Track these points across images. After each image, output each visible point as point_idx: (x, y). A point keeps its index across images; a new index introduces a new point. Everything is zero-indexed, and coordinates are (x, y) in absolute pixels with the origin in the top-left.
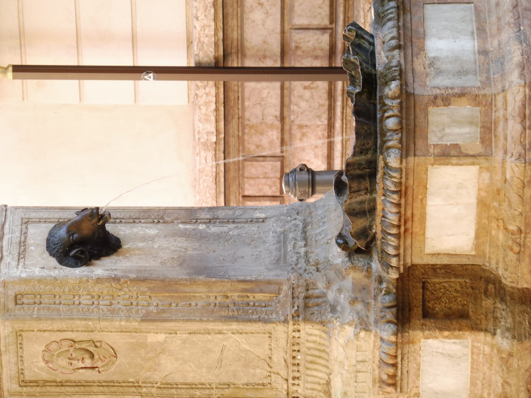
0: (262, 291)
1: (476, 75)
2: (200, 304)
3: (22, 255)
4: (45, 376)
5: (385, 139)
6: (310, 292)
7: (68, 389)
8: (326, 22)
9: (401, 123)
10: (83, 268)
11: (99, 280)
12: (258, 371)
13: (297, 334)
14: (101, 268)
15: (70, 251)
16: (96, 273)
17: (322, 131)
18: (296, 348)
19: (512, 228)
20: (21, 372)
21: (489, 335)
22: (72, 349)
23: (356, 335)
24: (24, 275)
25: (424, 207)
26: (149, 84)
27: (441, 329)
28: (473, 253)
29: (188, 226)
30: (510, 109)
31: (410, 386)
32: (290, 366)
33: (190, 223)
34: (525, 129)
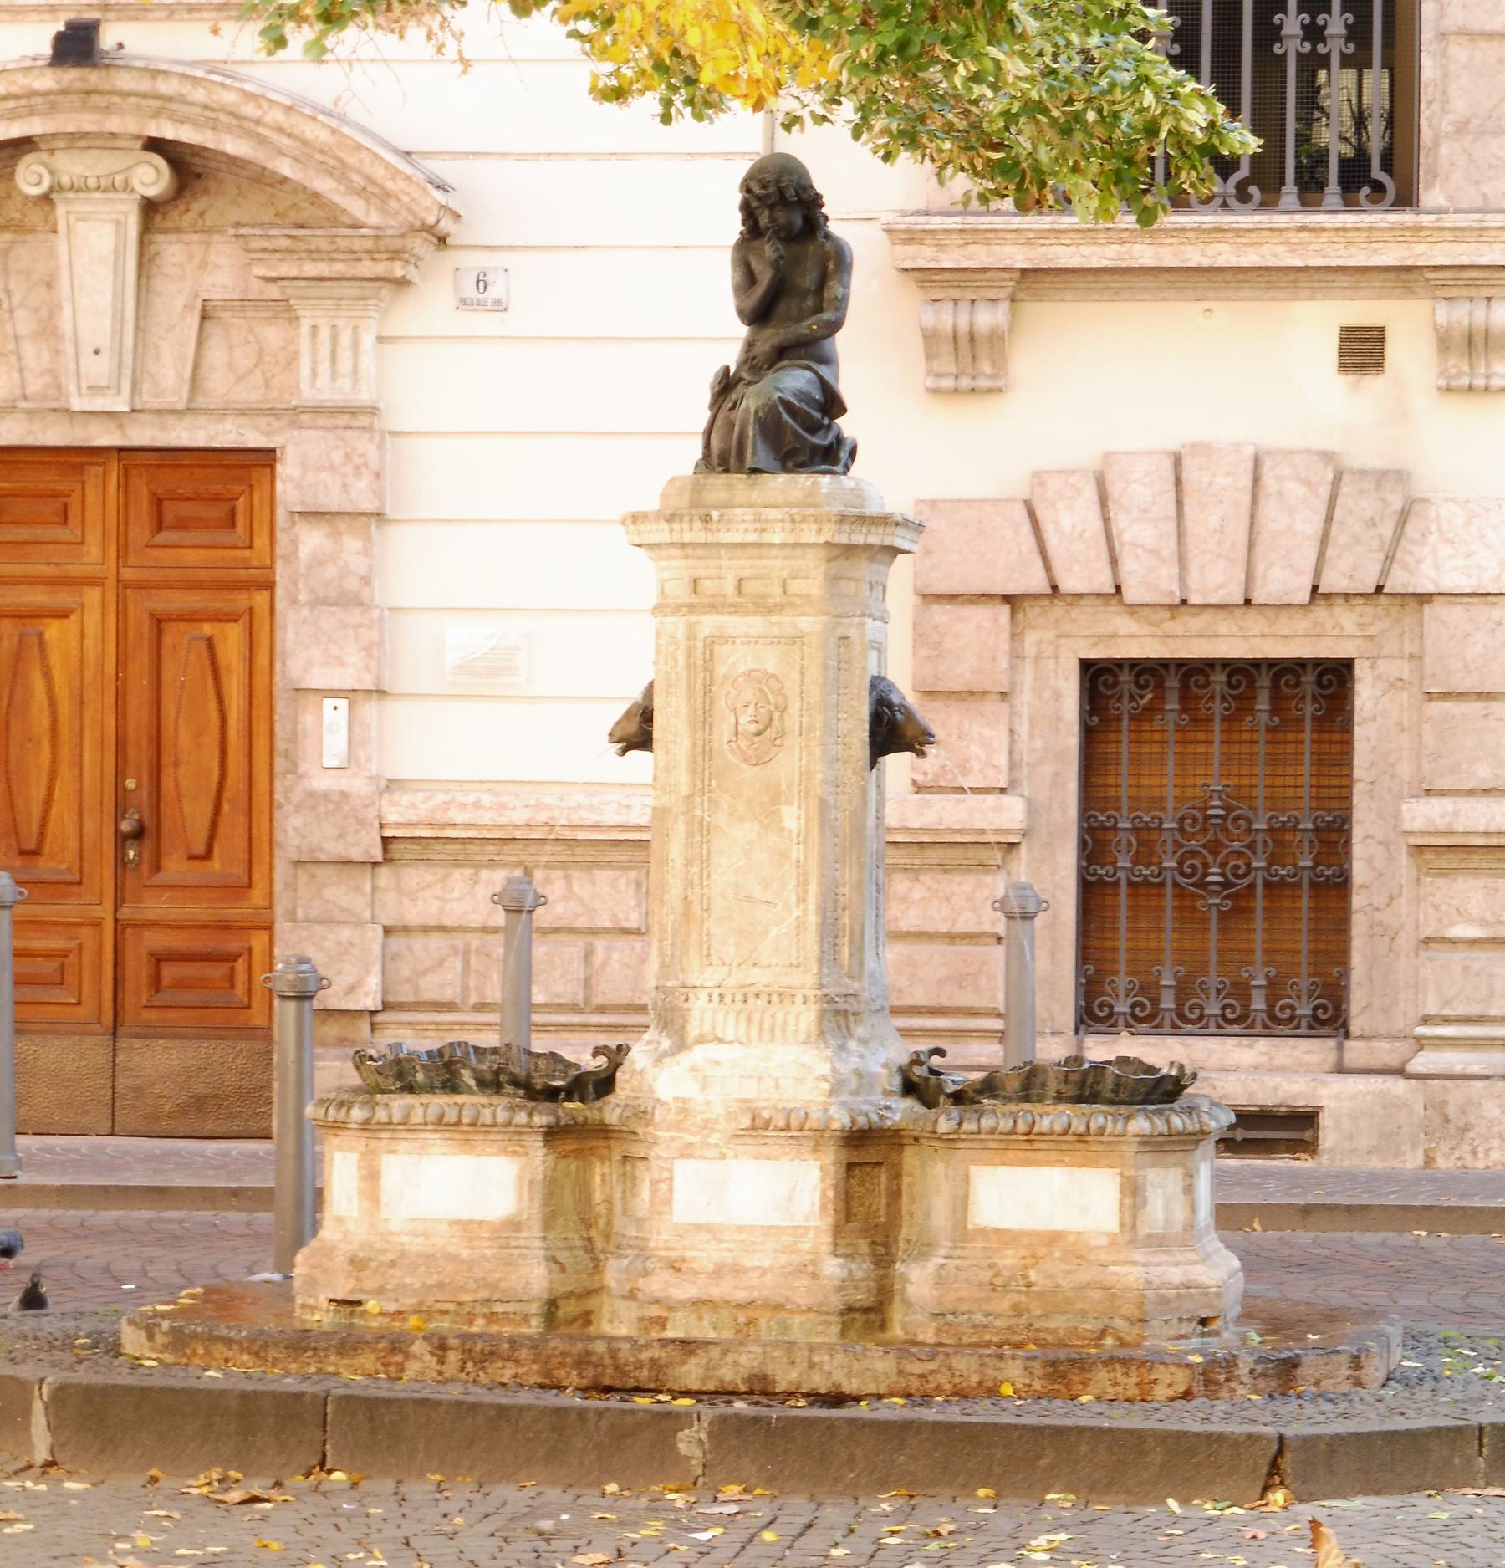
0: (851, 955)
2: (837, 874)
6: (852, 1018)
7: (700, 700)
8: (598, 1000)
9: (1179, 1134)
12: (732, 949)
13: (799, 1000)
18: (775, 998)
19: (1033, 1275)
20: (729, 640)
21: (830, 1248)
23: (824, 1078)
28: (970, 1227)
31: (740, 1148)
32: (744, 990)
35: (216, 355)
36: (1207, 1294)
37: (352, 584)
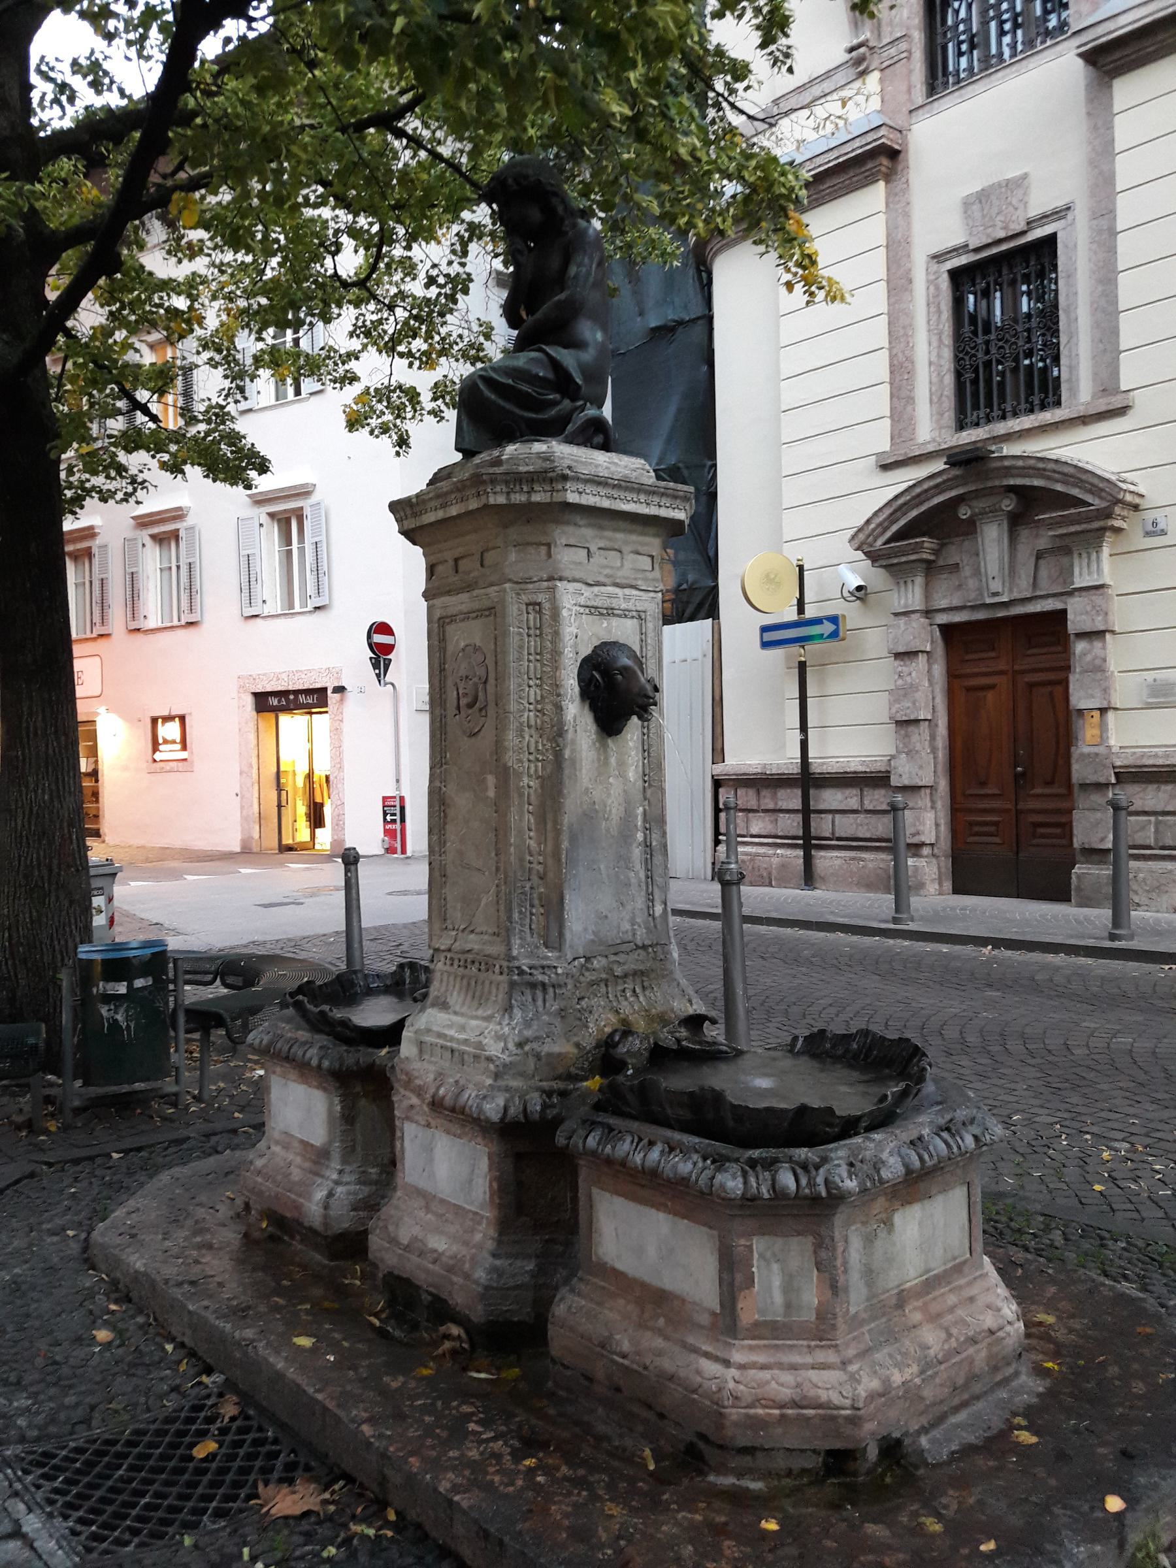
1: (868, 1300)
3: (594, 610)
4: (450, 648)
5: (759, 1168)
10: (577, 689)
11: (559, 708)
14: (576, 713)
15: (600, 672)
16: (570, 706)
17: (773, 832)
22: (475, 679)
24: (565, 613)
25: (658, 1206)
26: (797, 736)
27: (499, 1179)
29: (640, 818)
30: (813, 1375)
33: (645, 820)
34: (782, 1406)
35: (1043, 573)
36: (833, 1418)
37: (1098, 662)
